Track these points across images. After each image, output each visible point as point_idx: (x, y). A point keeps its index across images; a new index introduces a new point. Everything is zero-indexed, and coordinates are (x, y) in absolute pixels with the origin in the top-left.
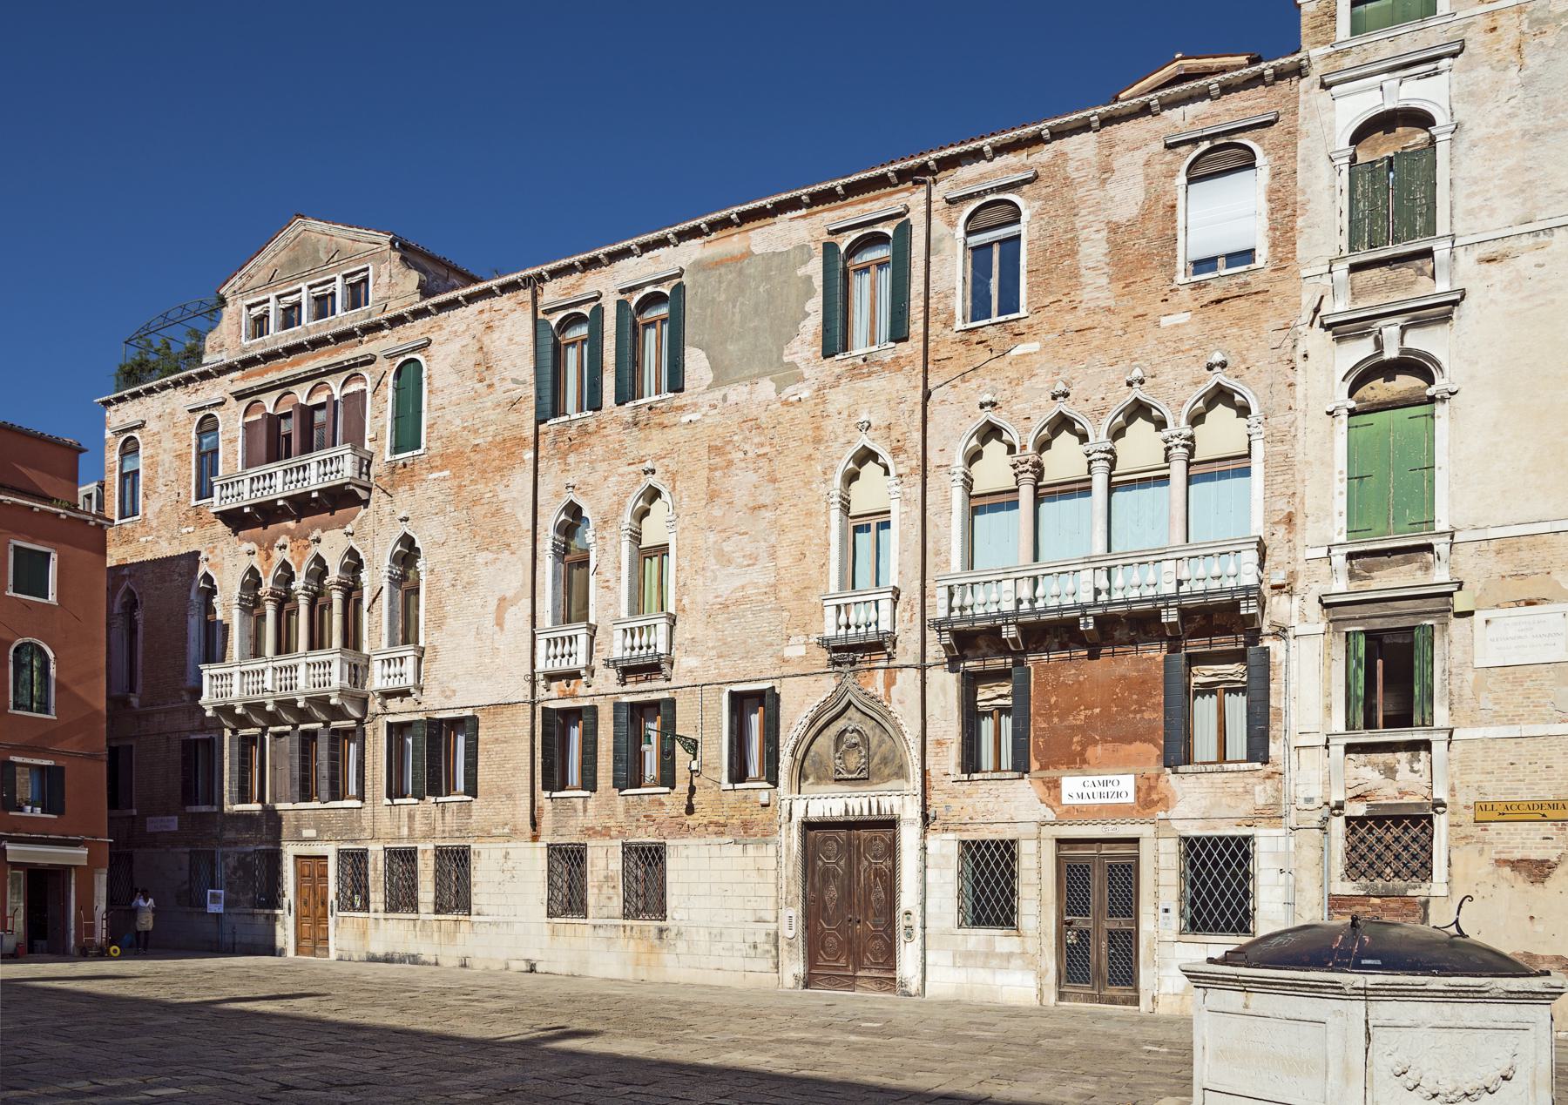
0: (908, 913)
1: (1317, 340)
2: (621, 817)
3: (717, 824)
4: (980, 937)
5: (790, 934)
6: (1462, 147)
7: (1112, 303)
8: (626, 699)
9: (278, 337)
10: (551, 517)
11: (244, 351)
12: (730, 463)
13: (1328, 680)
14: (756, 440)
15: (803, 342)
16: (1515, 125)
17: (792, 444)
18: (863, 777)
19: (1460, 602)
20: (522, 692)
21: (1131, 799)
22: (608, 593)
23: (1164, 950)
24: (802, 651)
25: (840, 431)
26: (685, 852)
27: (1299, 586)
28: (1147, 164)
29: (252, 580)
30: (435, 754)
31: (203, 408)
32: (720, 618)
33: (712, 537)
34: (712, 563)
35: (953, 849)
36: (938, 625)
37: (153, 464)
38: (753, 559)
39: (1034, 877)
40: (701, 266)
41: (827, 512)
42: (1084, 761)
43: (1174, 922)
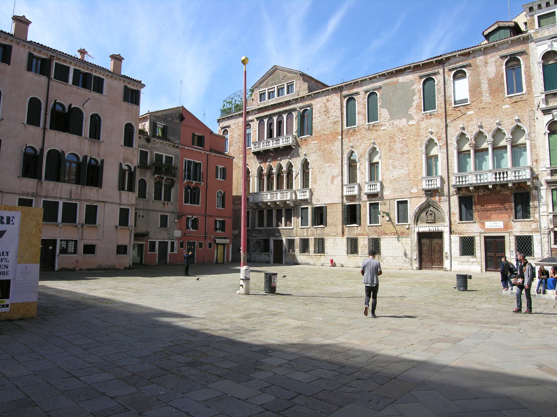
1: (539, 114)
2: (367, 231)
4: (465, 258)
7: (490, 101)
9: (268, 102)
11: (259, 105)
12: (395, 141)
17: (412, 136)
18: (434, 222)
20: (339, 200)
21: (502, 227)
24: (416, 191)
28: (496, 62)
29: (260, 170)
30: (320, 216)
33: (391, 161)
34: (391, 168)
35: (458, 239)
36: (453, 186)
37: (232, 137)
39: (479, 245)
42: (490, 218)
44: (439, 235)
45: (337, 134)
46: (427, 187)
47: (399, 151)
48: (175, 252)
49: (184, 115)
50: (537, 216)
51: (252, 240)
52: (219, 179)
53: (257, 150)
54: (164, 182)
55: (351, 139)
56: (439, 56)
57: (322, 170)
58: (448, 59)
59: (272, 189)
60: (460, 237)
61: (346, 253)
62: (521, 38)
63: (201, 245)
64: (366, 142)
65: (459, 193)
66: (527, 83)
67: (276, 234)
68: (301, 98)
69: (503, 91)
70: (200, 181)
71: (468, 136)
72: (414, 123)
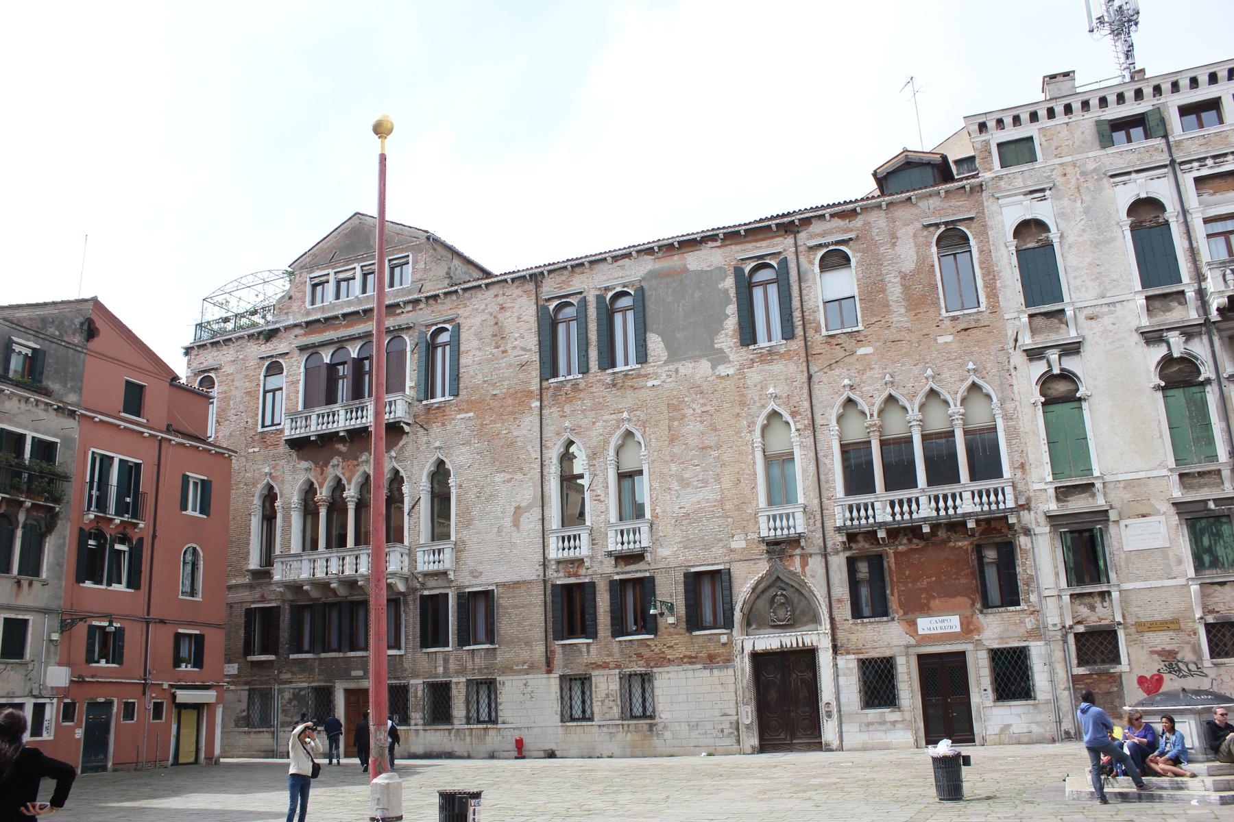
0: (828, 704)
1: (1018, 358)
2: (617, 656)
3: (690, 657)
4: (873, 713)
5: (748, 722)
6: (1066, 246)
7: (909, 325)
8: (617, 577)
10: (554, 453)
11: (308, 313)
12: (684, 416)
13: (1055, 559)
14: (701, 401)
15: (726, 335)
16: (1086, 237)
17: (725, 405)
19: (1113, 515)
21: (958, 629)
22: (602, 505)
23: (988, 712)
24: (743, 544)
25: (756, 398)
26: (668, 676)
27: (1033, 505)
28: (915, 236)
29: (310, 490)
31: (272, 356)
32: (684, 522)
33: (674, 467)
34: (675, 485)
36: (839, 529)
37: (226, 398)
38: (705, 483)
40: (652, 275)
41: (753, 453)
42: (929, 609)
43: (990, 695)
44: (808, 656)
45: (529, 394)
46: (772, 533)
47: (693, 441)
48: (47, 736)
49: (99, 324)
50: (1033, 598)
51: (281, 691)
52: (190, 512)
53: (299, 433)
54: (22, 517)
55: (567, 408)
56: (784, 215)
57: (488, 491)
58: (806, 222)
59: (342, 543)
60: (859, 660)
61: (558, 718)
62: (968, 188)
63: (129, 710)
64: (607, 417)
65: (850, 548)
66: (986, 287)
67: (354, 673)
68: (427, 298)
69: (936, 303)
70: (134, 516)
71: (863, 405)
72: (731, 371)
